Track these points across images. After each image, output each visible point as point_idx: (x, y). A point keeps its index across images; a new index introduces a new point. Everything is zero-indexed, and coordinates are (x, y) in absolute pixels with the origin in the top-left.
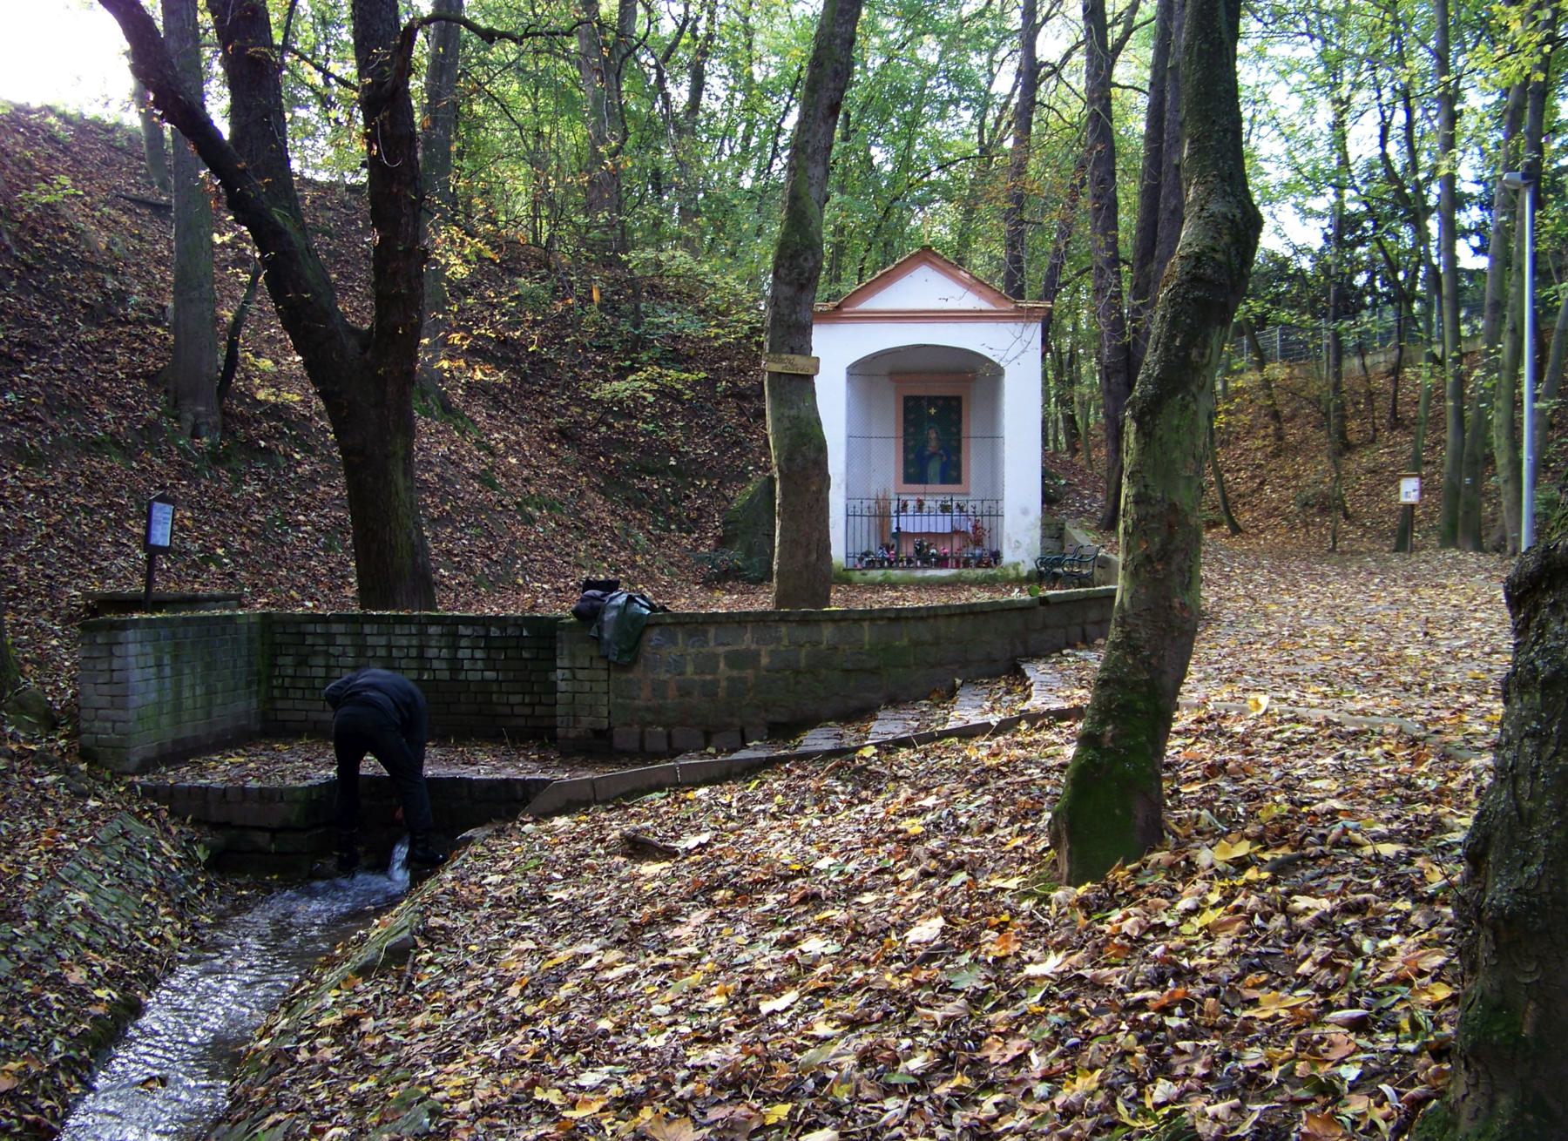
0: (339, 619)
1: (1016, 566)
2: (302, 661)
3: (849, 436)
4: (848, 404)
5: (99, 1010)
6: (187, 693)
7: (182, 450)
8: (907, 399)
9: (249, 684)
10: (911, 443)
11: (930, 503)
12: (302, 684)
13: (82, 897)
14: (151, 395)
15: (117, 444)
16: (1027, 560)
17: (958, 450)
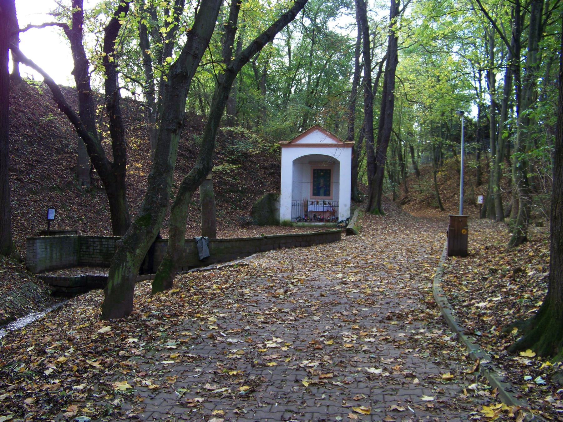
0: (96, 237)
2: (88, 248)
3: (293, 182)
4: (293, 172)
5: (4, 318)
6: (54, 255)
7: (78, 189)
9: (74, 253)
11: (321, 202)
12: (87, 253)
13: (11, 298)
14: (71, 174)
15: (59, 188)
17: (329, 186)
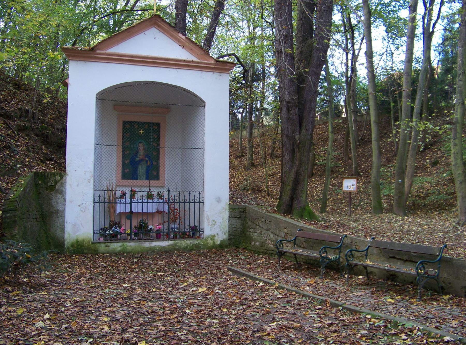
1: (213, 237)
4: (96, 122)
8: (125, 123)
10: (127, 153)
11: (141, 193)
16: (220, 233)
17: (157, 158)
